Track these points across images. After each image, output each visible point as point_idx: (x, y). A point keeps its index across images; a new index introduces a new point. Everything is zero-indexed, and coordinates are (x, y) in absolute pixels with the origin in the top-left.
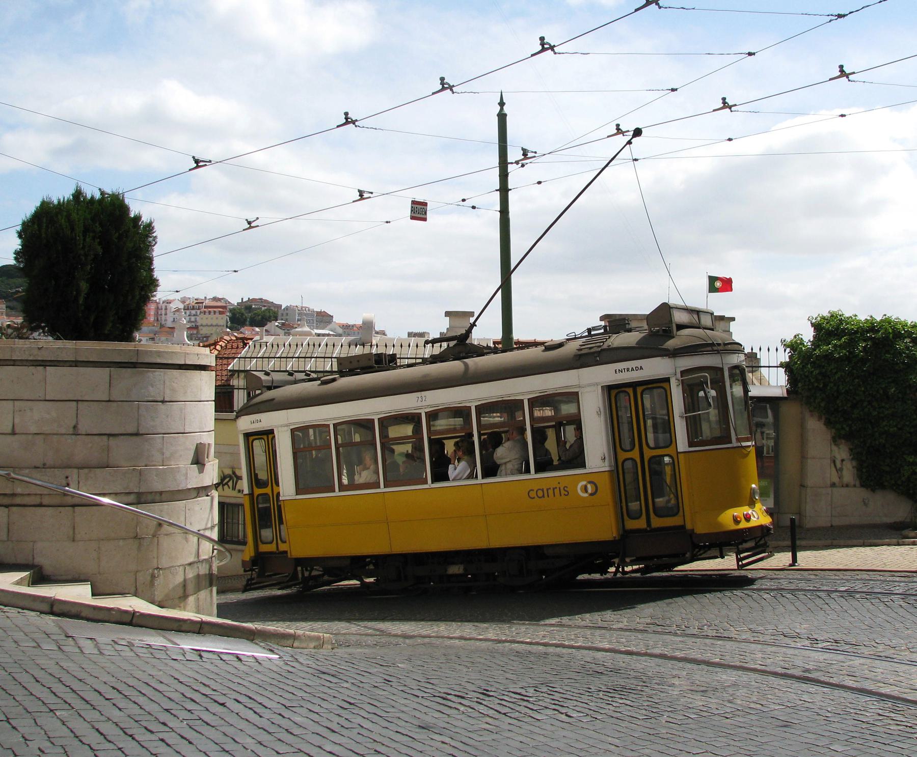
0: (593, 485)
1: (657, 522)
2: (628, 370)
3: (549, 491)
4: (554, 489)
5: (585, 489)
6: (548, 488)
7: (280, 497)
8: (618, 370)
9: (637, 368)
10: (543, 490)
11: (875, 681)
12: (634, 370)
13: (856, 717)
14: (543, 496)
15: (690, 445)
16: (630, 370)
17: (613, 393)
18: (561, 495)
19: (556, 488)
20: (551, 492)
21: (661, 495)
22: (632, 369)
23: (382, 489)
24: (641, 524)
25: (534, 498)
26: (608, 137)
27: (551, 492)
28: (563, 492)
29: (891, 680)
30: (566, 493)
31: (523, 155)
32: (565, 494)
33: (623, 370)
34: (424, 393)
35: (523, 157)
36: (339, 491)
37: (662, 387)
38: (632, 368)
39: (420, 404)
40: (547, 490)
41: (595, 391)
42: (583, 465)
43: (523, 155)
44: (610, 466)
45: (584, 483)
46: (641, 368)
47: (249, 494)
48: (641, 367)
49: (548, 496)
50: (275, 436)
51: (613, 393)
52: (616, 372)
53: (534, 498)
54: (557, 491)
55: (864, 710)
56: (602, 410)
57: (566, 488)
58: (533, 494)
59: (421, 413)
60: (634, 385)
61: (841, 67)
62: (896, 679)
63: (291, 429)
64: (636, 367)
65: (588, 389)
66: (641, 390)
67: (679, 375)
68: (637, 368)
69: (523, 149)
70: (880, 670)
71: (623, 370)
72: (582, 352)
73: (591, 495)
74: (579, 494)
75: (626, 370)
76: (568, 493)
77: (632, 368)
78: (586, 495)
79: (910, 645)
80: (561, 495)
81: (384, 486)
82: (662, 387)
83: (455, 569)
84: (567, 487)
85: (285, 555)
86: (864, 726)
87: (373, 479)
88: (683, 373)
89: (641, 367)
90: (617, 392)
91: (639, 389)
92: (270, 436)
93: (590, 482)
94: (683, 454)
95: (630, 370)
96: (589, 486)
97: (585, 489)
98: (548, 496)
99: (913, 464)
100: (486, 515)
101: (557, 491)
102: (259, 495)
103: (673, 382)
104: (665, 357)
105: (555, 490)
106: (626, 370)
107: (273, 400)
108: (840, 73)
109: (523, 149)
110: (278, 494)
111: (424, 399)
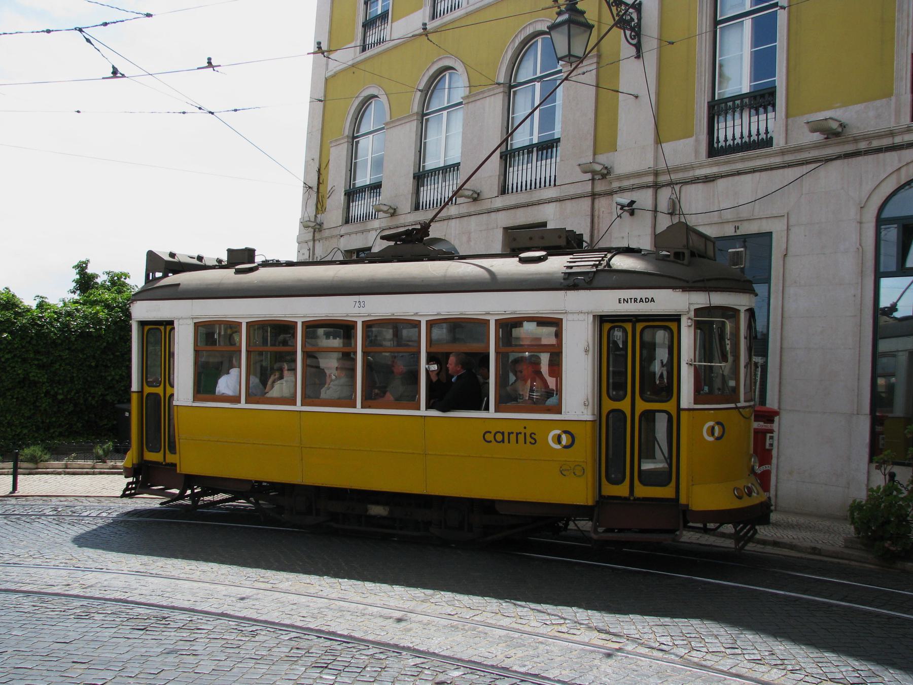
0: (570, 436)
1: (642, 491)
2: (635, 300)
3: (511, 435)
4: (517, 434)
5: (558, 439)
6: (510, 432)
7: (174, 402)
8: (622, 300)
9: (647, 300)
10: (503, 433)
11: (14, 582)
12: (643, 302)
13: (17, 610)
14: (503, 441)
15: (696, 402)
16: (638, 301)
17: (607, 326)
18: (525, 443)
19: (520, 433)
20: (513, 437)
21: (651, 456)
22: (641, 300)
23: (243, 405)
24: (622, 490)
25: (490, 442)
26: (198, 68)
27: (513, 437)
28: (529, 439)
29: (28, 581)
30: (533, 441)
31: (112, 73)
32: (530, 442)
33: (629, 300)
34: (362, 298)
35: (112, 75)
36: (302, 405)
37: (620, 327)
38: (641, 299)
39: (356, 310)
40: (509, 434)
41: (584, 320)
42: (558, 410)
43: (112, 73)
44: (593, 414)
45: (558, 432)
46: (653, 300)
47: (138, 392)
48: (652, 298)
49: (509, 442)
50: (174, 328)
51: (607, 326)
52: (619, 301)
53: (490, 442)
54: (521, 437)
55: (20, 604)
56: (591, 346)
57: (533, 436)
58: (489, 437)
59: (562, 319)
60: (634, 319)
61: (209, 59)
62: (31, 579)
63: (195, 323)
64: (646, 298)
65: (576, 317)
66: (641, 327)
67: (692, 314)
68: (647, 300)
69: (113, 67)
70: (15, 574)
71: (629, 300)
72: (574, 270)
73: (565, 447)
74: (550, 446)
75: (633, 300)
76: (536, 441)
77: (641, 299)
78: (558, 447)
79: (31, 553)
80: (525, 443)
81: (194, 399)
82: (620, 327)
83: (377, 510)
84: (535, 434)
85: (173, 468)
86: (26, 615)
87: (286, 393)
88: (698, 312)
89: (652, 298)
90: (647, 326)
91: (640, 326)
92: (169, 328)
93: (565, 432)
94: (687, 412)
95: (638, 301)
96: (564, 437)
97: (558, 439)
98: (509, 442)
99: (1, 416)
100: (302, 447)
101: (521, 437)
102: (149, 394)
103: (684, 322)
104: (677, 290)
105: (519, 435)
106: (633, 300)
107: (179, 285)
108: (207, 65)
109: (113, 67)
110: (172, 395)
111: (362, 304)
